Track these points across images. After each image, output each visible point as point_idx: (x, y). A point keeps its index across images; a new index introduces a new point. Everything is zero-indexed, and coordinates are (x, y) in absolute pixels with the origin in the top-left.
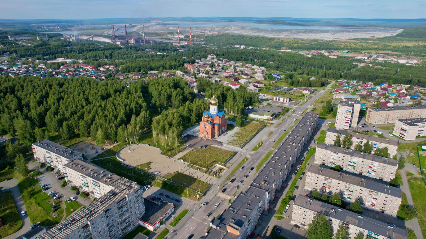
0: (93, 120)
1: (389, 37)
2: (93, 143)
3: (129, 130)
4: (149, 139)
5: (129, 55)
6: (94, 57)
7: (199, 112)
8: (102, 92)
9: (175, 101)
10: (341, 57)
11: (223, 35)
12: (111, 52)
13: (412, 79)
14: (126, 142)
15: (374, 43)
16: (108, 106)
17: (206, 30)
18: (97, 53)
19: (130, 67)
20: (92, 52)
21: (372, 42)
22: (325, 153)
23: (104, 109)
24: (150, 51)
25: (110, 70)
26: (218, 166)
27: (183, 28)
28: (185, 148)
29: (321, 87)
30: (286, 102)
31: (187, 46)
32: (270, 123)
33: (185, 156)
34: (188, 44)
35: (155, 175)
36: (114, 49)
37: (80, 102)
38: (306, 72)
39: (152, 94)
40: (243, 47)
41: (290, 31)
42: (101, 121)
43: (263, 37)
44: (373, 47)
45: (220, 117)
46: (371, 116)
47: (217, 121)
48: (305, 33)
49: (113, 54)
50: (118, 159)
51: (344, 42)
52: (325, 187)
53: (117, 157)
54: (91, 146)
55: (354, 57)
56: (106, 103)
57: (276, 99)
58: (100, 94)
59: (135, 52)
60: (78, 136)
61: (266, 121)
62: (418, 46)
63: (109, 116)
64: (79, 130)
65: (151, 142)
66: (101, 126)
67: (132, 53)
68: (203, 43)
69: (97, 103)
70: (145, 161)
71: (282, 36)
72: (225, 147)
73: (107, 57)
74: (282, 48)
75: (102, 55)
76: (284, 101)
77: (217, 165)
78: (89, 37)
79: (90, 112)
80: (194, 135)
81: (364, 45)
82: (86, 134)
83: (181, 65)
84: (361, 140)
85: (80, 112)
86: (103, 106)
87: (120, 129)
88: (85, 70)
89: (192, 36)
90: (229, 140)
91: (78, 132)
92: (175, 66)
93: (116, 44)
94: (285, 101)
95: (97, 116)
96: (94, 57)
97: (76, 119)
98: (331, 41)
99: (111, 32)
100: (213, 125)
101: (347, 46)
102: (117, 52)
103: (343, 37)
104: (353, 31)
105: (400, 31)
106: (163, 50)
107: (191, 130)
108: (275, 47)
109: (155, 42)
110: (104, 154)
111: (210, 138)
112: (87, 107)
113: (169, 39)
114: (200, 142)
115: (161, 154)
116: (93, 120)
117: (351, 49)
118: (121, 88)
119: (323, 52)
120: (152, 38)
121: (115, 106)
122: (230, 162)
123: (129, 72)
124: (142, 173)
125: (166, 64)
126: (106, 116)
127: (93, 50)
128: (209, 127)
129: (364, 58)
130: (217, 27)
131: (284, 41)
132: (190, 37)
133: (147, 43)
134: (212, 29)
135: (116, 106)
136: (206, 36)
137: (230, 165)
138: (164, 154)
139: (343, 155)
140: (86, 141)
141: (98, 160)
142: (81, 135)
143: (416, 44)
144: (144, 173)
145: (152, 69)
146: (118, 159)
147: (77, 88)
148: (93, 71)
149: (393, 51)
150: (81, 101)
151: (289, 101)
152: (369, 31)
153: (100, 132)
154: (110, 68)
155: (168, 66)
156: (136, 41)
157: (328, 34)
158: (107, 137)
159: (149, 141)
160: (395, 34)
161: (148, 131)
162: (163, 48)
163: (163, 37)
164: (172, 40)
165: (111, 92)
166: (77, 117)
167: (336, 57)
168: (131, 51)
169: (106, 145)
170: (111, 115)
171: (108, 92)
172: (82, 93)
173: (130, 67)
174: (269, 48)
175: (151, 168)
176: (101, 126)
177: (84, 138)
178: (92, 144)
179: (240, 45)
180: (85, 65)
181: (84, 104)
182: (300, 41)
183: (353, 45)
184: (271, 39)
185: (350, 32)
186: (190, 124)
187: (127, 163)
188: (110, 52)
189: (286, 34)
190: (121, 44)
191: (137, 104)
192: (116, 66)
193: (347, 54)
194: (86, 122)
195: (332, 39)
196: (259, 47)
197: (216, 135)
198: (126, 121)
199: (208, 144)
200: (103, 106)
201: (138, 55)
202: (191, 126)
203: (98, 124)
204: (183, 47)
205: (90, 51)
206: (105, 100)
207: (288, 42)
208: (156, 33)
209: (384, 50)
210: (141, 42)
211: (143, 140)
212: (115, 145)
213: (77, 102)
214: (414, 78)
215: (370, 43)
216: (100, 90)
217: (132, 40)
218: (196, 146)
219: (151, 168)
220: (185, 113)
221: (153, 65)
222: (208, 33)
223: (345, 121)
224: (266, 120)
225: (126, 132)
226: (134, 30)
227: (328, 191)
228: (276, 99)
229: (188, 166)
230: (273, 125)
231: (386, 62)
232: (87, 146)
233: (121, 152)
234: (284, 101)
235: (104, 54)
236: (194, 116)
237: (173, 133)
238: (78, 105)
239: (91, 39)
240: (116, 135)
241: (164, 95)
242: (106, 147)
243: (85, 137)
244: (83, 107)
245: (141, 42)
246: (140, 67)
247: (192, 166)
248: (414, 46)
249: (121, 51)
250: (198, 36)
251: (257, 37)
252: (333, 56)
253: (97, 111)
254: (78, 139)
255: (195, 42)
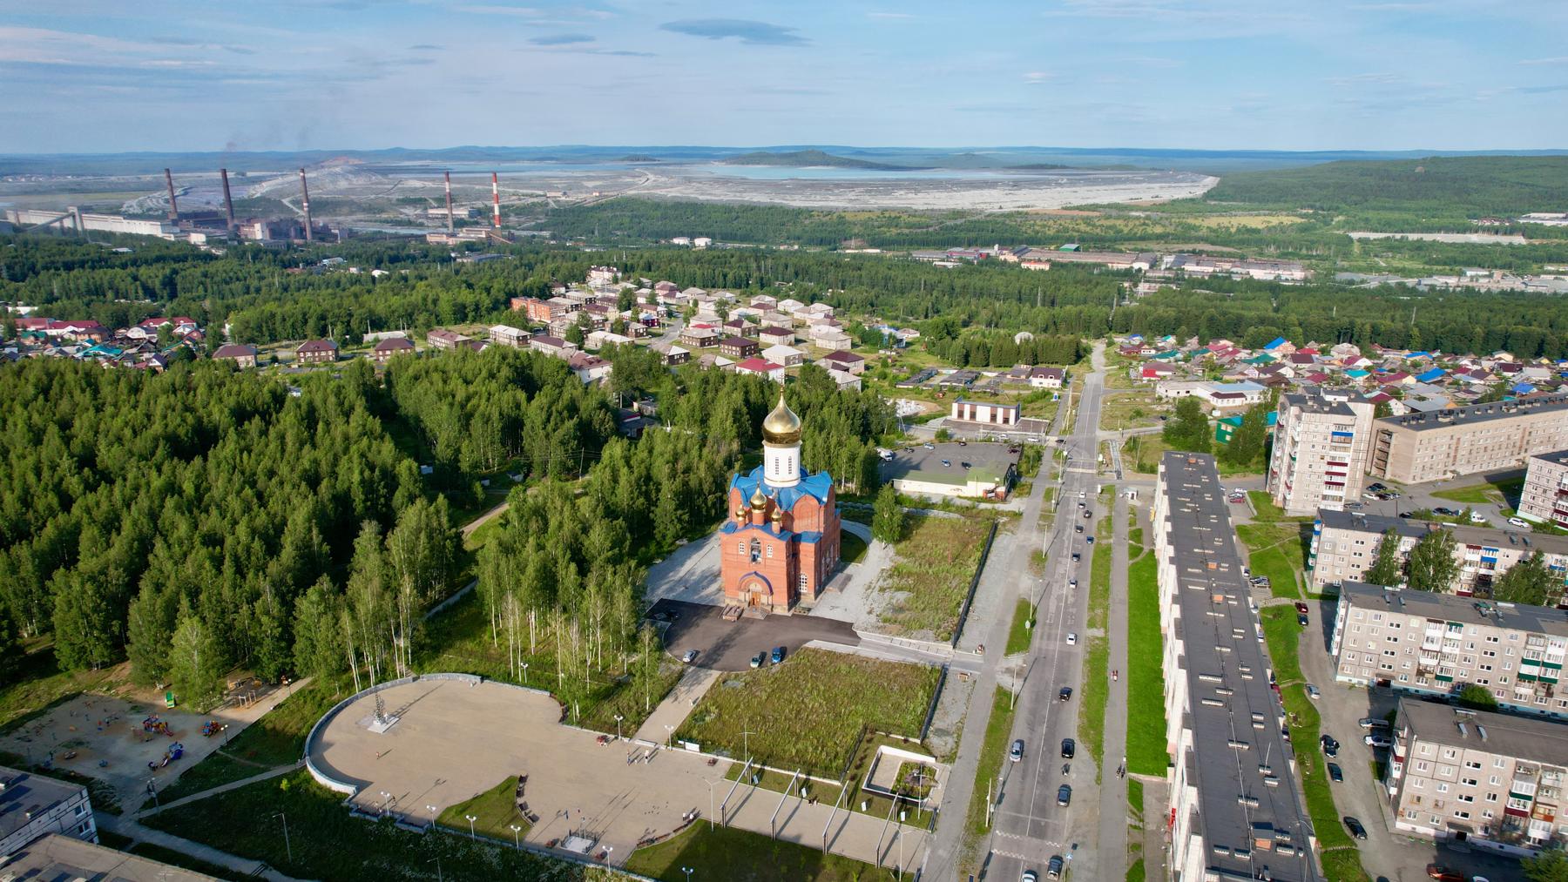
0: (137, 564)
1: (1185, 200)
2: (142, 696)
3: (361, 610)
4: (469, 645)
5: (254, 283)
6: (89, 292)
7: (685, 484)
8: (165, 417)
9: (545, 443)
10: (1063, 266)
11: (619, 204)
12: (168, 271)
13: (1352, 324)
14: (349, 675)
15: (1148, 218)
16: (218, 485)
17: (551, 188)
18: (102, 276)
19: (279, 317)
20: (75, 272)
21: (1142, 215)
22: (1394, 632)
23: (196, 504)
24: (338, 266)
25: (181, 337)
26: (893, 757)
27: (459, 181)
28: (681, 676)
29: (1076, 362)
30: (1006, 421)
31: (487, 244)
32: (1007, 514)
33: (697, 716)
34: (488, 237)
35: (576, 856)
36: (184, 259)
37: (46, 474)
38: (984, 314)
39: (418, 420)
40: (701, 242)
41: (862, 185)
42: (189, 569)
43: (772, 209)
44: (1149, 230)
45: (819, 500)
46: (1392, 451)
47: (811, 522)
48: (917, 191)
49: (178, 279)
50: (321, 779)
51: (1054, 217)
52: (1524, 814)
53: (311, 769)
54: (138, 722)
55: (1105, 265)
56: (205, 468)
57: (961, 414)
58: (157, 428)
59: (278, 270)
60: (45, 664)
61: (983, 506)
62: (1282, 228)
63: (229, 540)
64: (48, 628)
65: (486, 657)
66: (194, 594)
67: (265, 272)
68: (546, 234)
69: (154, 473)
70: (490, 780)
71: (836, 202)
72: (869, 645)
73: (150, 293)
74: (845, 244)
75: (125, 284)
76: (994, 417)
77: (885, 750)
78: (57, 215)
79: (111, 525)
80: (695, 599)
81: (1120, 223)
82: (98, 653)
83: (499, 307)
84: (1490, 555)
85: (50, 530)
86: (188, 488)
87: (308, 604)
88: (52, 340)
89: (502, 207)
90: (878, 611)
91: (45, 642)
92: (477, 308)
93: (188, 243)
94: (1000, 419)
95: (159, 545)
96: (89, 292)
97: (28, 568)
98: (1010, 215)
99: (157, 200)
100: (794, 542)
101: (1066, 230)
102: (198, 272)
103: (1046, 200)
104: (1072, 183)
105: (1210, 182)
106: (394, 260)
107: (665, 575)
108: (821, 242)
109: (352, 234)
110: (226, 762)
111: (782, 610)
112: (91, 497)
113: (410, 223)
114: (738, 631)
115: (564, 719)
116: (137, 564)
117: (1082, 240)
118: (267, 397)
119: (994, 251)
120: (339, 222)
121: (253, 485)
122: (938, 722)
123: (274, 339)
124: (491, 855)
125: (435, 302)
126: (213, 540)
127: (82, 265)
128: (774, 552)
129: (1136, 266)
130: (589, 178)
131: (849, 217)
132: (497, 212)
133: (322, 239)
134: (574, 185)
135: (260, 485)
136: (553, 210)
137: (950, 741)
138: (581, 724)
139: (1492, 631)
140: (101, 692)
141: (196, 805)
142: (64, 654)
143: (1274, 221)
144: (505, 852)
145: (378, 324)
146: (321, 779)
147: (18, 409)
148: (94, 343)
149: (1213, 243)
150: (53, 468)
151: (1017, 418)
152: (1119, 181)
153: (190, 636)
154: (179, 330)
155: (445, 307)
156: (275, 231)
157: (993, 192)
158: (235, 654)
159: (471, 654)
160: (1199, 192)
161: (451, 601)
162: (392, 253)
163: (384, 216)
164: (421, 225)
165: (216, 416)
166: (34, 555)
167: (1046, 267)
168: (259, 266)
169: (227, 705)
170: (242, 530)
171: (199, 420)
172: (53, 429)
173: (279, 317)
174: (801, 245)
175: (534, 819)
176: (194, 594)
177: (83, 677)
178: (137, 708)
179: (692, 236)
180: (47, 320)
181: (73, 484)
182: (905, 217)
183: (1083, 227)
184: (798, 213)
185: (1061, 185)
186: (653, 548)
187: (379, 798)
188: (164, 276)
189: (851, 196)
190: (208, 242)
191: (372, 469)
192: (203, 320)
193: (1077, 255)
194: (93, 579)
195: (1009, 207)
196: (763, 242)
197: (807, 589)
198: (330, 561)
199: (785, 638)
200: (188, 488)
201: (292, 279)
202: (659, 554)
203: (171, 587)
204: (470, 247)
205: (69, 267)
206: (198, 461)
207: (864, 224)
208: (351, 203)
209: (1187, 240)
210: (293, 233)
211: (437, 650)
212: (281, 695)
213: (31, 478)
214: (1359, 321)
215: (1138, 218)
216: (158, 412)
217: (258, 226)
218: (728, 657)
219: (534, 819)
220: (623, 495)
221: (381, 309)
222: (556, 197)
223: (1327, 478)
224: (980, 500)
225: (345, 617)
226: (258, 191)
227: (1537, 832)
228: (961, 414)
229: (732, 774)
230: (1024, 522)
231: (1213, 276)
232: (112, 724)
233: (329, 734)
234: (994, 417)
235: (135, 278)
236: (671, 506)
237: (606, 600)
238: (37, 489)
239: (68, 223)
240: (287, 637)
241: (487, 420)
242: (231, 713)
243: (89, 665)
244: (66, 502)
245: (293, 233)
246: (323, 317)
247: (761, 773)
248: (1269, 229)
249: (211, 268)
250: (521, 211)
251: (751, 208)
252: (1036, 262)
253: (154, 516)
254: (42, 686)
255: (517, 233)
